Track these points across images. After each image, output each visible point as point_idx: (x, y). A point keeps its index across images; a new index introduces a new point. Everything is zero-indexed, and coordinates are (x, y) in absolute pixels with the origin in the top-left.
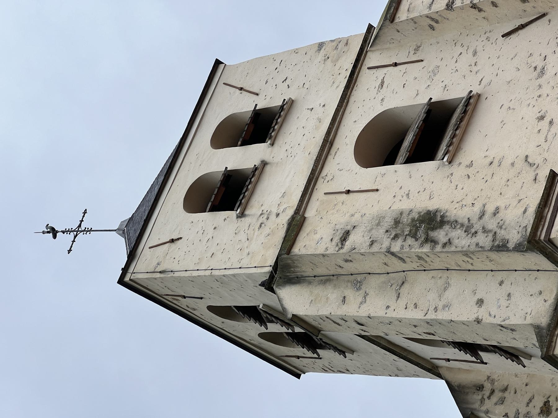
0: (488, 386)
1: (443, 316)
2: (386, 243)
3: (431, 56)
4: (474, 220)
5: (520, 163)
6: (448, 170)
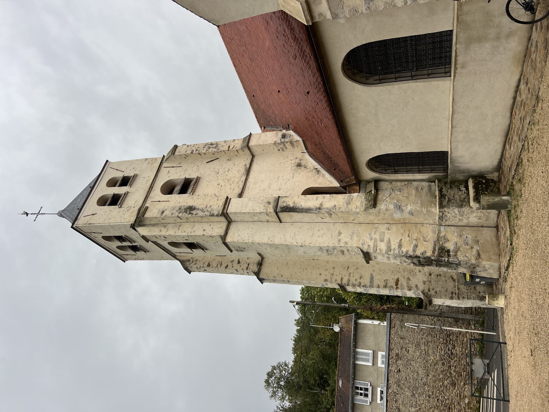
0: (191, 260)
1: (193, 234)
2: (177, 214)
3: (184, 166)
4: (204, 208)
5: (213, 196)
6: (192, 196)
